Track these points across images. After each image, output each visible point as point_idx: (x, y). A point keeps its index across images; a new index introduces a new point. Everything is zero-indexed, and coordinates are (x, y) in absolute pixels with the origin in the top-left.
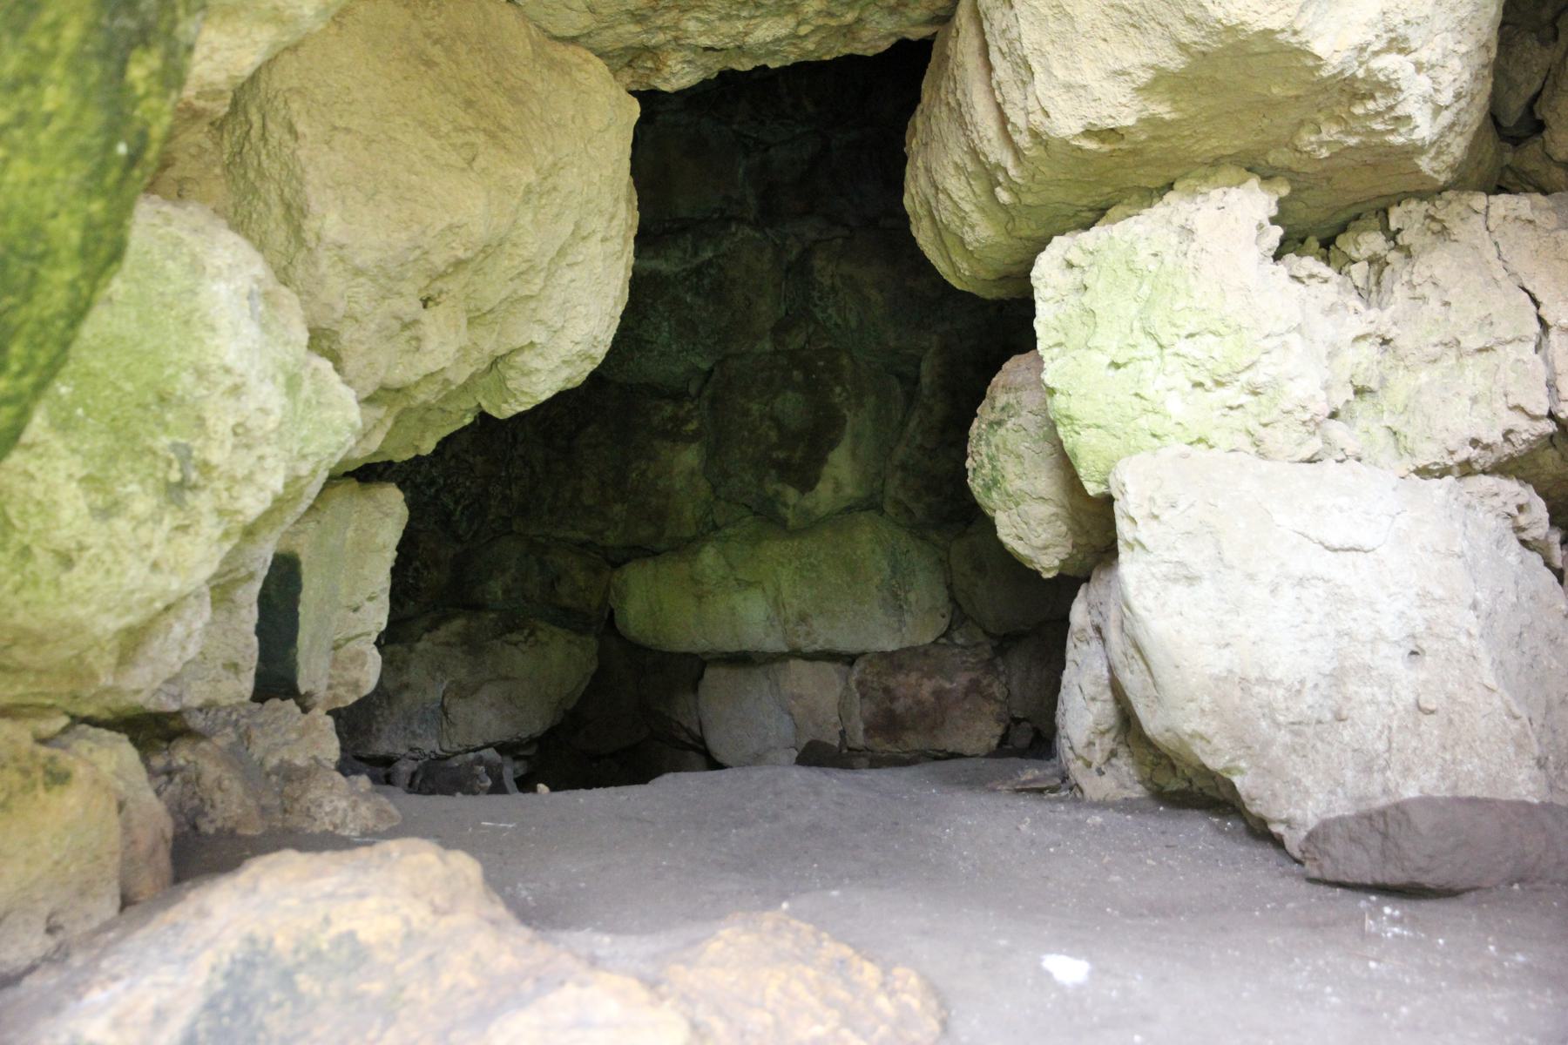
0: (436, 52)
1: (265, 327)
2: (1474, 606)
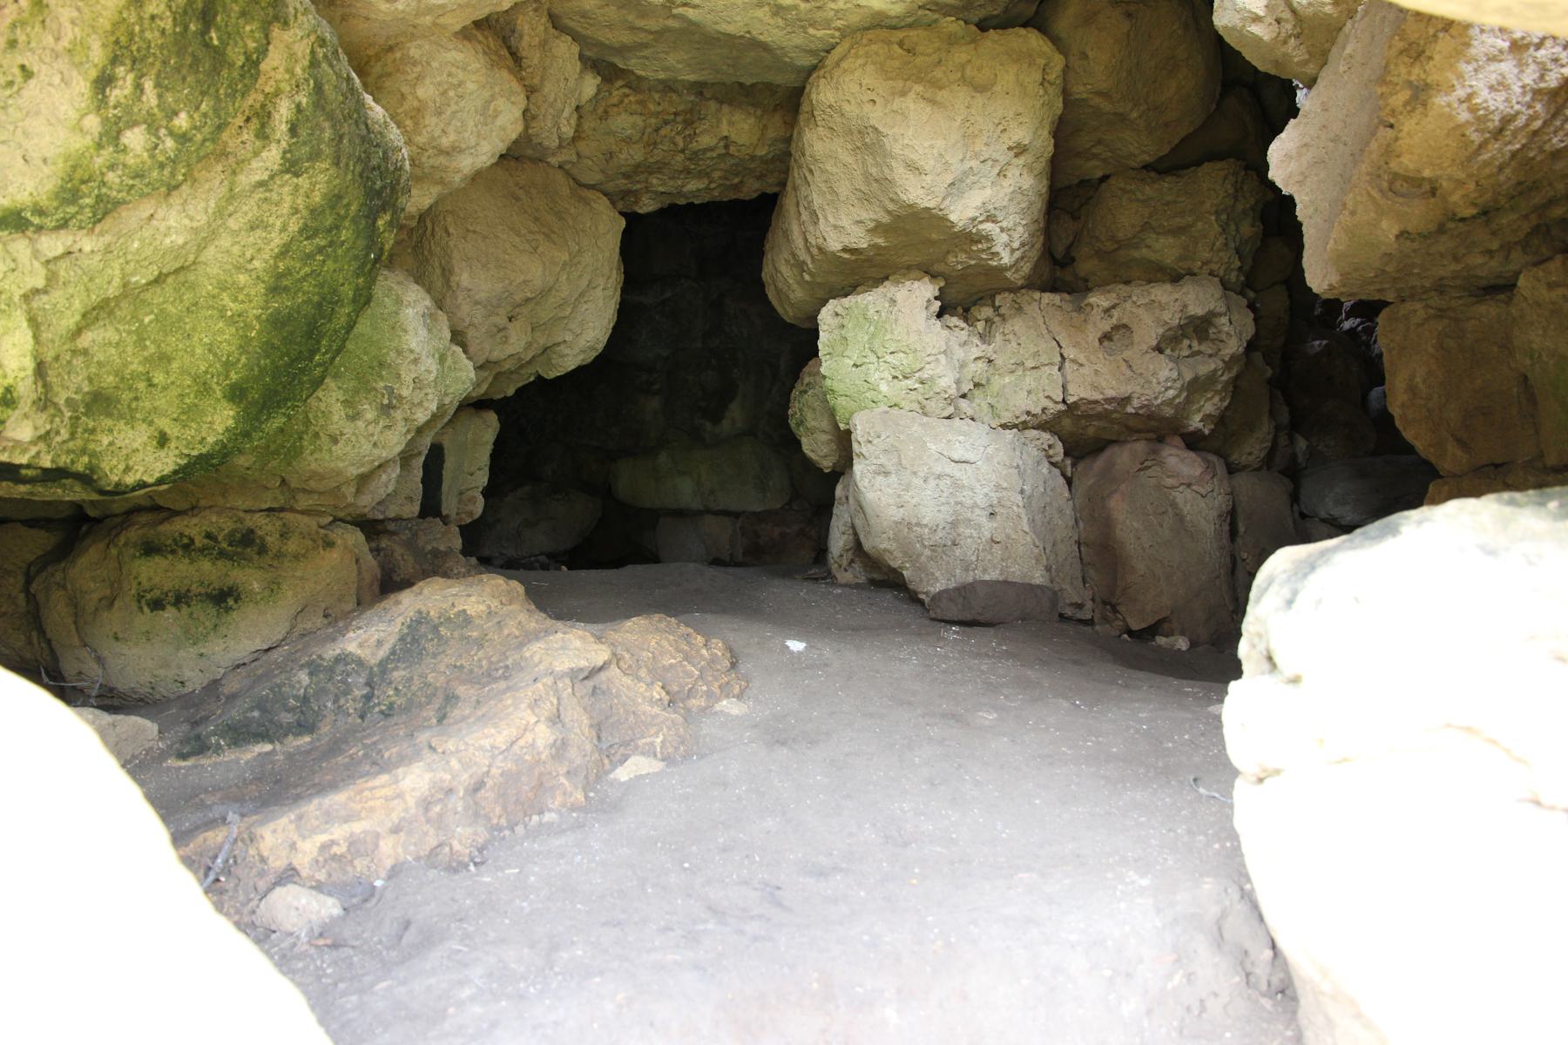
0: (520, 193)
1: (430, 331)
2: (1022, 492)
